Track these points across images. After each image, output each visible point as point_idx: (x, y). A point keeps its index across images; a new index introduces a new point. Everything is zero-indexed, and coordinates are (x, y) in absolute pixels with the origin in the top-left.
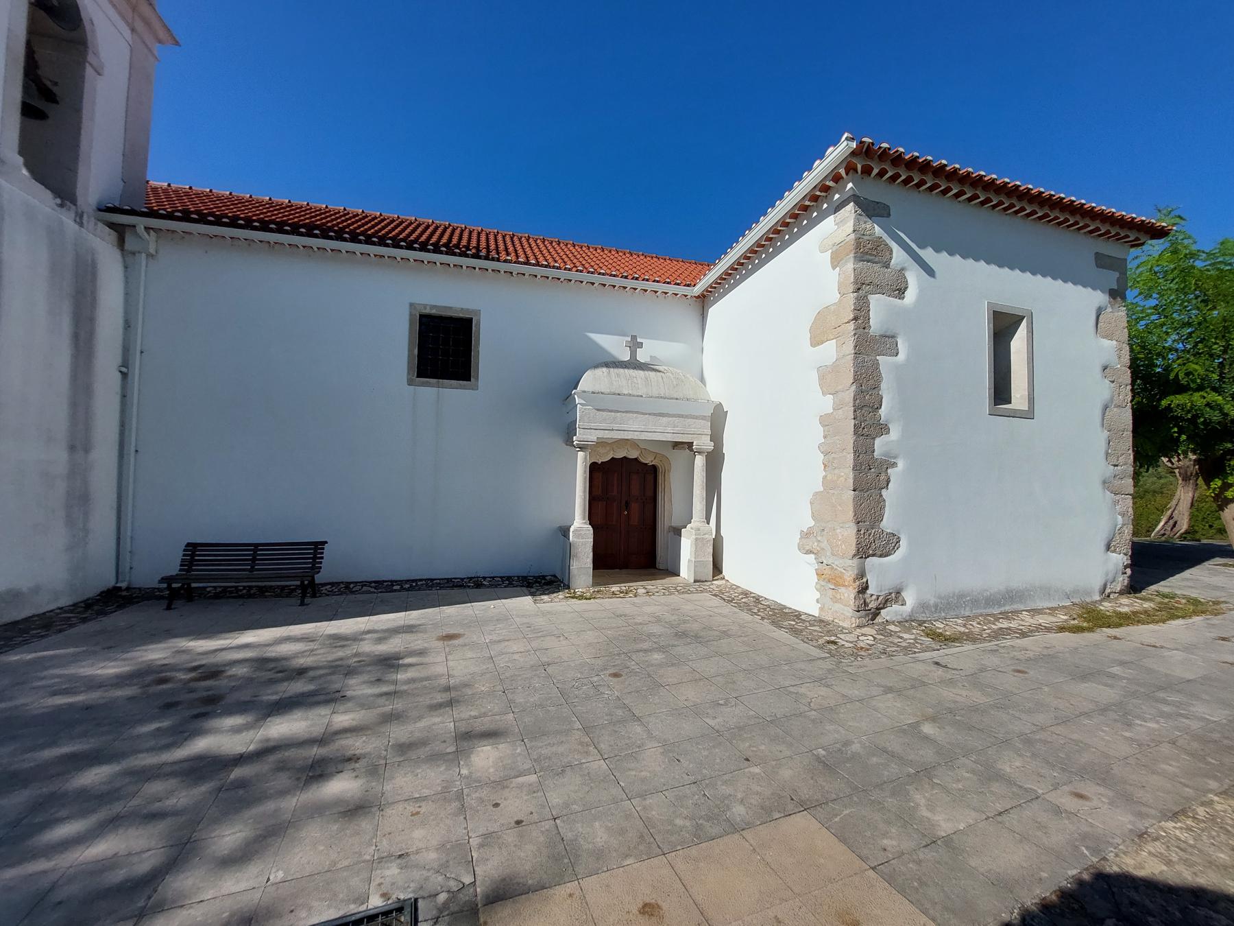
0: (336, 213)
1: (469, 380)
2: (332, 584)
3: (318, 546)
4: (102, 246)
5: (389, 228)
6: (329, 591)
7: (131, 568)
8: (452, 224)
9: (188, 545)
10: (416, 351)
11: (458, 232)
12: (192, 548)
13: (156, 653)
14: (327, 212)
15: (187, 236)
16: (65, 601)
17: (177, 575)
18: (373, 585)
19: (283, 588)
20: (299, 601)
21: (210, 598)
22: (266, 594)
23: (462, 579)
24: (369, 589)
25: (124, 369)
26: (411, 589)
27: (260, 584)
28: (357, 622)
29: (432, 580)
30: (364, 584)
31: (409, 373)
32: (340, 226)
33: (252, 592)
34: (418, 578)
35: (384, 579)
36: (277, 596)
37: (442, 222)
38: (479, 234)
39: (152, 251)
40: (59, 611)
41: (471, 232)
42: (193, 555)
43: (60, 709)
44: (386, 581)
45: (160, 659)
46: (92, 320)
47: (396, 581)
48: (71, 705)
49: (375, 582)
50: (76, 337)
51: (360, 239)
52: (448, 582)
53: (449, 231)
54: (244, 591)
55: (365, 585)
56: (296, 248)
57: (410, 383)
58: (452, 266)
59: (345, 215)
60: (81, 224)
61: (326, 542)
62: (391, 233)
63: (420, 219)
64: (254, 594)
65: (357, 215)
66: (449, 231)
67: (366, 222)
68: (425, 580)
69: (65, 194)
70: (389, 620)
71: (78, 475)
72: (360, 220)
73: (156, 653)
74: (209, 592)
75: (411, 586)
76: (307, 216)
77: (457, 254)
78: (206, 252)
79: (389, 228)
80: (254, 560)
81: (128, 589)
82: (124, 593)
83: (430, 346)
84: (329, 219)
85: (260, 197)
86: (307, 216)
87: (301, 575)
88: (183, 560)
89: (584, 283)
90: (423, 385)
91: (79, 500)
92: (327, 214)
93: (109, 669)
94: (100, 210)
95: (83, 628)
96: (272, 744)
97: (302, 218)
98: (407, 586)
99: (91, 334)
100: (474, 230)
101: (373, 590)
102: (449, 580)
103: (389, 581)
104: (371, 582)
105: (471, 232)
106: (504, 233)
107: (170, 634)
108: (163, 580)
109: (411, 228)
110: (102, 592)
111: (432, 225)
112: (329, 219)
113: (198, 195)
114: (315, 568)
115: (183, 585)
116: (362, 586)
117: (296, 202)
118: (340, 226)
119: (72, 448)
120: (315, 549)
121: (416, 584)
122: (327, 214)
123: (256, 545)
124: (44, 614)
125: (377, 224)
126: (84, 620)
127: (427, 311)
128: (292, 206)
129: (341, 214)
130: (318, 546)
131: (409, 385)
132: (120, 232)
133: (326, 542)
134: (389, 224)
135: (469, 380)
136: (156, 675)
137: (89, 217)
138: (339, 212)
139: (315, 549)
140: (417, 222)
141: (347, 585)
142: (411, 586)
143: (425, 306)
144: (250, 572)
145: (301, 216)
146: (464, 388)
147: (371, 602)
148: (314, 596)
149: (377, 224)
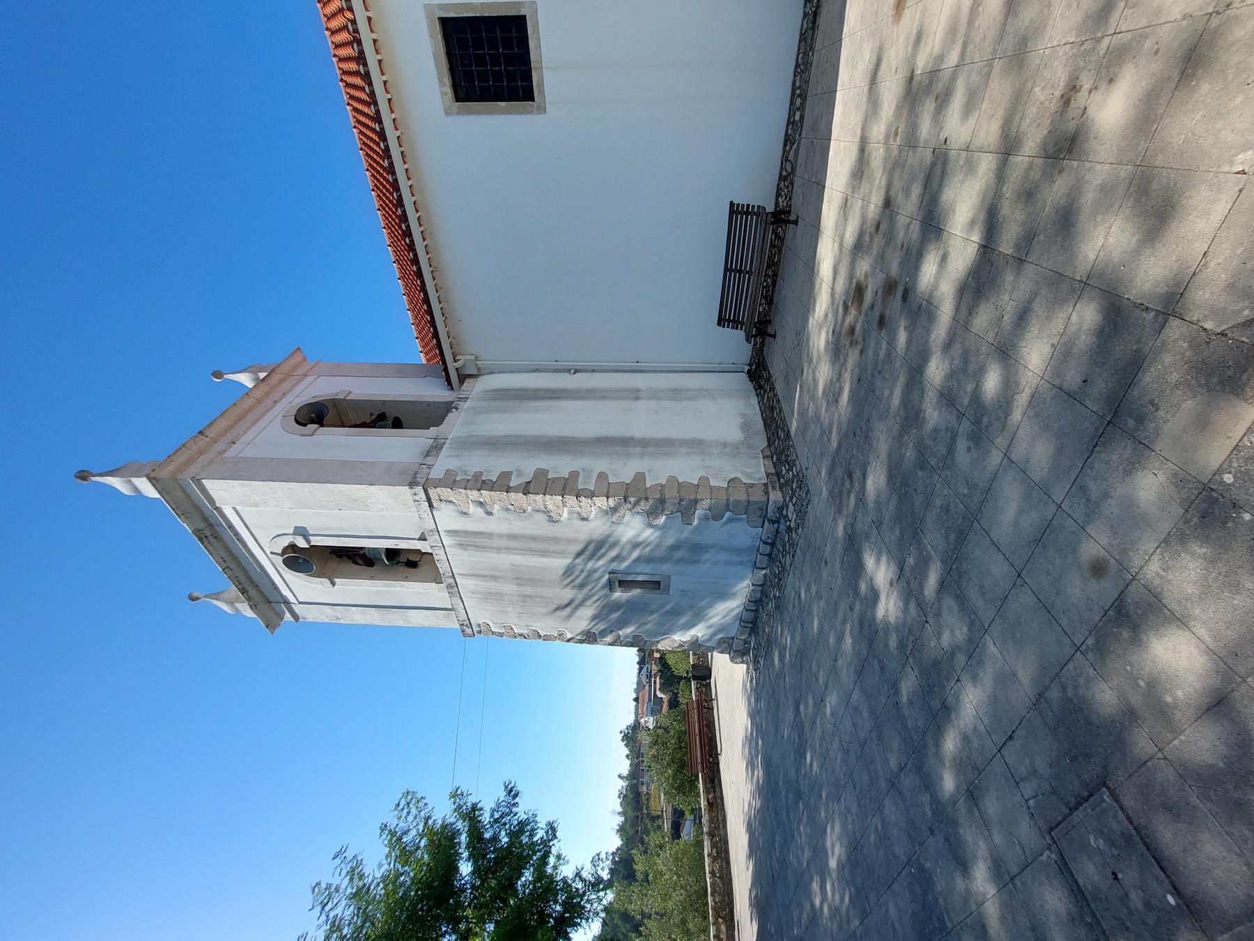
0: (381, 198)
1: (524, 17)
2: (778, 195)
3: (734, 210)
4: (476, 388)
5: (375, 157)
6: (785, 199)
7: (733, 364)
8: (340, 79)
9: (719, 324)
10: (502, 104)
11: (345, 66)
12: (721, 321)
13: (819, 340)
14: (388, 226)
15: (451, 335)
16: (754, 401)
17: (745, 332)
18: (788, 148)
19: (773, 246)
20: (792, 226)
21: (770, 309)
22: (775, 261)
23: (805, 15)
24: (792, 152)
25: (572, 371)
26: (804, 97)
27: (765, 267)
28: (835, 154)
29: (797, 66)
30: (785, 158)
31: (530, 112)
32: (391, 190)
33: (771, 273)
34: (790, 87)
35: (783, 134)
36: (780, 251)
37: (344, 93)
38: (333, 32)
39: (473, 357)
40: (761, 404)
41: (337, 46)
42: (729, 321)
43: (852, 398)
44: (787, 132)
45: (827, 333)
46: (536, 390)
47: (789, 118)
48: (851, 390)
49: (785, 145)
50: (551, 398)
51: (406, 227)
52: (805, 40)
53: (350, 80)
54: (769, 280)
55: (787, 157)
56: (430, 259)
57: (542, 110)
58: (422, 228)
59: (378, 188)
60: (467, 398)
61: (731, 202)
62: (375, 140)
63: (339, 75)
64: (773, 271)
65: (378, 195)
66: (350, 80)
67: (377, 173)
68: (795, 76)
69: (448, 407)
70: (843, 113)
71: (655, 395)
72: (381, 191)
73: (819, 340)
74: (764, 309)
75: (799, 96)
76: (399, 244)
77: (398, 193)
78: (460, 321)
79: (375, 157)
80: (740, 271)
81: (750, 365)
82: (754, 367)
83: (491, 83)
84: (393, 223)
85: (411, 318)
86: (399, 244)
87: (763, 225)
88: (733, 328)
89: (369, 14)
90: (542, 92)
91: (676, 394)
92: (390, 225)
93: (823, 372)
94: (452, 389)
95: (779, 390)
96: (982, 217)
97: (402, 248)
98: (798, 101)
99: (547, 390)
100: (333, 42)
101: (795, 146)
102: (803, 38)
103: (787, 127)
104: (784, 151)
105: (337, 46)
106: (331, 46)
107: (801, 334)
108: (748, 341)
109: (368, 142)
110: (750, 380)
111: (352, 105)
112: (393, 223)
113: (420, 333)
114: (759, 212)
115: (755, 327)
116: (787, 160)
117: (392, 257)
118: (391, 190)
119: (637, 398)
120: (738, 212)
121: (799, 88)
122: (390, 225)
123: (726, 270)
124: (761, 411)
125: (378, 172)
126: (773, 389)
127: (448, 90)
128: (397, 260)
129: (384, 212)
130: (734, 210)
131: (545, 112)
132: (463, 378)
133: (731, 202)
134: (372, 158)
135: (524, 17)
136: (841, 342)
137: (460, 394)
138: (394, 251)
139: (738, 212)
140: (357, 125)
141: (782, 178)
142: (799, 96)
143: (444, 94)
144: (752, 274)
145: (402, 250)
146: (536, 25)
147: (812, 142)
148: (789, 212)
149: (378, 172)
